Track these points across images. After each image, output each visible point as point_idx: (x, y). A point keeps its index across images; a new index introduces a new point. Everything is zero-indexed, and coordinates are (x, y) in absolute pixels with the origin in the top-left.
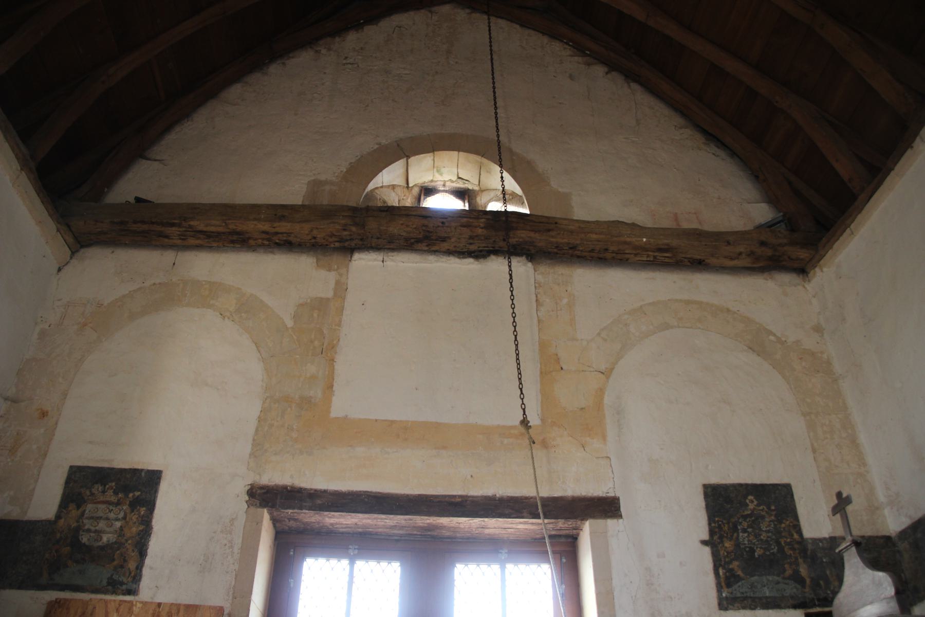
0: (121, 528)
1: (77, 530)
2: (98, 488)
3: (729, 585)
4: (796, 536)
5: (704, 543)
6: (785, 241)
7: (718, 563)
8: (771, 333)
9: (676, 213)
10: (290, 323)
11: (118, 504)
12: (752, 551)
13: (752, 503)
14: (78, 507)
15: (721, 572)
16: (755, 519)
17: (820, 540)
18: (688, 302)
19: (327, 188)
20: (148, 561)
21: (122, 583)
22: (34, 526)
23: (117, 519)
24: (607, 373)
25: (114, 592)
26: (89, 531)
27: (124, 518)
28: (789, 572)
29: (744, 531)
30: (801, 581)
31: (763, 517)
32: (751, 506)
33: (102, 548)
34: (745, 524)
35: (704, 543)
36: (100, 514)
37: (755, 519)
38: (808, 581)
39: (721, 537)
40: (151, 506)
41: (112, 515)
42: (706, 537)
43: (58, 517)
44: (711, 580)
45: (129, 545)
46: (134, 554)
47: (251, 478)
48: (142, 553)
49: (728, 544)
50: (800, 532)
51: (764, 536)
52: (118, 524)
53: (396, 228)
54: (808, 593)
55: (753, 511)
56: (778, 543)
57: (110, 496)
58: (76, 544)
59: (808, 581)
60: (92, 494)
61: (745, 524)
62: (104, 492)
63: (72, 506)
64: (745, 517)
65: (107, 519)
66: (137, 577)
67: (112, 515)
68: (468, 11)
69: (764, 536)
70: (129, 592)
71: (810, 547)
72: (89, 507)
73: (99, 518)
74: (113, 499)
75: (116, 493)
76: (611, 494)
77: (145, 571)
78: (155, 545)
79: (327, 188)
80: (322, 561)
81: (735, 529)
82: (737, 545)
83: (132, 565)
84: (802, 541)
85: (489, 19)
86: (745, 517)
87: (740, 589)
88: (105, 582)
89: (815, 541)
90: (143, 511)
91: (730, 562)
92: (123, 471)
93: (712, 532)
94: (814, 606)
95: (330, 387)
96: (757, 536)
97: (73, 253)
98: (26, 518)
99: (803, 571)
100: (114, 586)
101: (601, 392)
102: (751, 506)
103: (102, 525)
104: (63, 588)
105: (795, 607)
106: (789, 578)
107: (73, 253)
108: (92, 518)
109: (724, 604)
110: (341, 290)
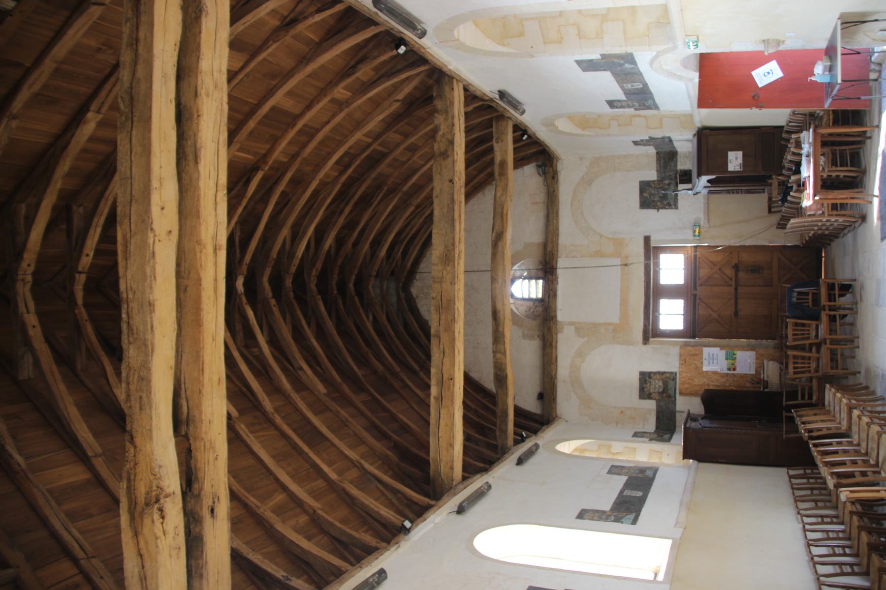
0: (658, 380)
1: (659, 393)
2: (646, 390)
3: (671, 205)
4: (656, 182)
5: (658, 211)
6: (551, 169)
7: (664, 208)
8: (583, 177)
9: (532, 203)
10: (585, 339)
11: (650, 383)
12: (661, 197)
13: (645, 195)
14: (651, 394)
15: (667, 207)
16: (651, 194)
17: (657, 174)
18: (572, 204)
19: (526, 332)
20: (667, 370)
21: (674, 377)
22: (658, 406)
23: (655, 382)
24: (601, 236)
25: (676, 378)
26: (659, 389)
27: (654, 380)
28: (667, 187)
29: (654, 198)
30: (669, 184)
31: (650, 192)
32: (647, 195)
33: (664, 384)
34: (652, 198)
35: (658, 211)
36: (654, 388)
37: (651, 194)
38: (670, 181)
39: (656, 206)
40: (650, 373)
41: (654, 384)
42: (656, 210)
43: (655, 399)
44: (669, 211)
45: (663, 377)
46: (665, 375)
47: (641, 344)
48: (665, 373)
49: (659, 204)
50: (655, 181)
51: (656, 193)
52: (656, 381)
53: (179, 374)
54: (673, 182)
55: (648, 195)
56: (658, 188)
57: (648, 385)
58: (663, 392)
59: (670, 181)
60: (648, 391)
61: (652, 198)
62: (647, 387)
63: (652, 396)
64: (650, 197)
65: (655, 385)
66: (672, 373)
67: (654, 384)
68: (415, 281)
69: (656, 193)
70: (676, 374)
71: (660, 179)
72: (652, 391)
73: (655, 388)
74: (649, 384)
75: (647, 384)
76: (643, 238)
77: (670, 371)
78: (662, 369)
79: (526, 332)
80: (660, 323)
81: (654, 201)
82: (659, 201)
83: (668, 375)
84: (658, 181)
85: (420, 273)
86: (650, 197)
87: (672, 203)
88: (673, 382)
89: (658, 177)
90: (652, 375)
91: (664, 204)
92: (640, 383)
93: (655, 208)
94: (677, 181)
95: (609, 324)
96: (656, 195)
97: (560, 418)
98: (655, 409)
99: (667, 182)
100: (674, 379)
101: (608, 238)
102: (647, 195)
103: (657, 386)
104: (675, 393)
105: (677, 187)
106: (669, 187)
107: (560, 418)
108: (655, 389)
109: (676, 207)
110: (571, 323)
